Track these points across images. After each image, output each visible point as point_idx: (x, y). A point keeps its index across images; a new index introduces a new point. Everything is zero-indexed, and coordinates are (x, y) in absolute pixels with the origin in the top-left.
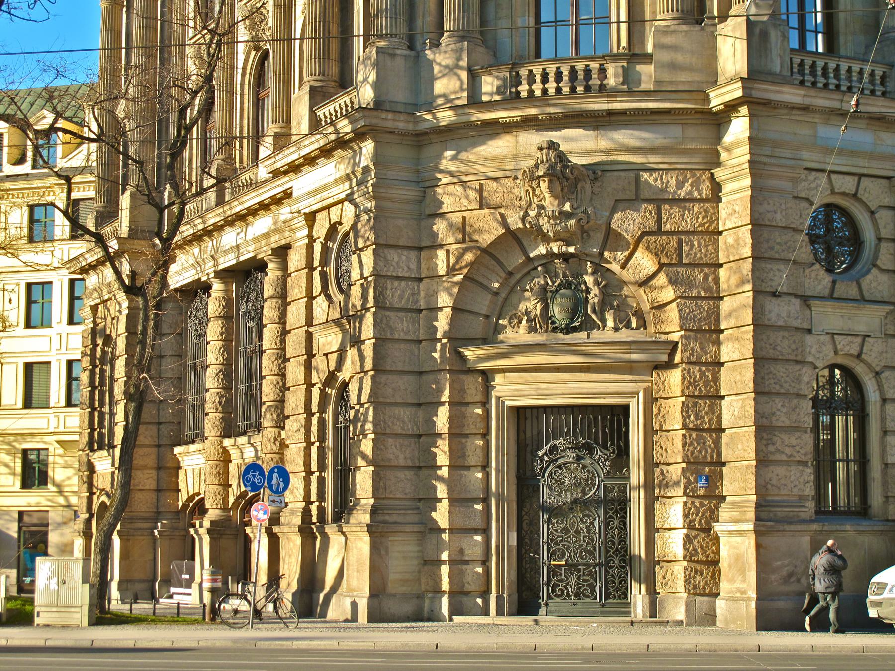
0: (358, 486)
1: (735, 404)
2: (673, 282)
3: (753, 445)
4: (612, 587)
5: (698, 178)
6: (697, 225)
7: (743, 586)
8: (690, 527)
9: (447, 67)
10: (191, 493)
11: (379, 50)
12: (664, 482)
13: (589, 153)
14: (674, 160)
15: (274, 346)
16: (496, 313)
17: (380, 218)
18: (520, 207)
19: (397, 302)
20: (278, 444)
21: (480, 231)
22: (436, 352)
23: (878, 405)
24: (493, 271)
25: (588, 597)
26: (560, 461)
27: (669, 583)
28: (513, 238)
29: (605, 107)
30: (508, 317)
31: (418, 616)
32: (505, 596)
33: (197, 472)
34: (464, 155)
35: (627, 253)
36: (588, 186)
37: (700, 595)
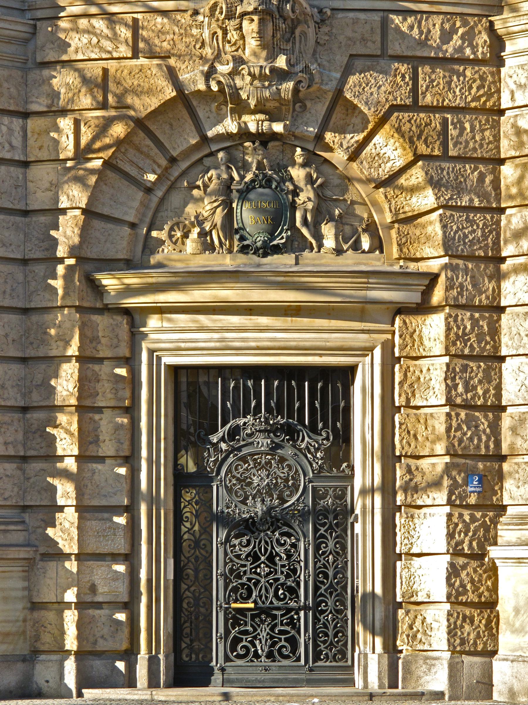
2: (434, 183)
4: (324, 642)
5: (472, 28)
6: (469, 99)
8: (456, 552)
12: (412, 484)
18: (201, 58)
22: (55, 277)
24: (148, 156)
25: (287, 657)
26: (245, 451)
27: (419, 636)
30: (167, 227)
32: (161, 656)
35: (360, 137)
36: (311, 32)
37: (469, 653)
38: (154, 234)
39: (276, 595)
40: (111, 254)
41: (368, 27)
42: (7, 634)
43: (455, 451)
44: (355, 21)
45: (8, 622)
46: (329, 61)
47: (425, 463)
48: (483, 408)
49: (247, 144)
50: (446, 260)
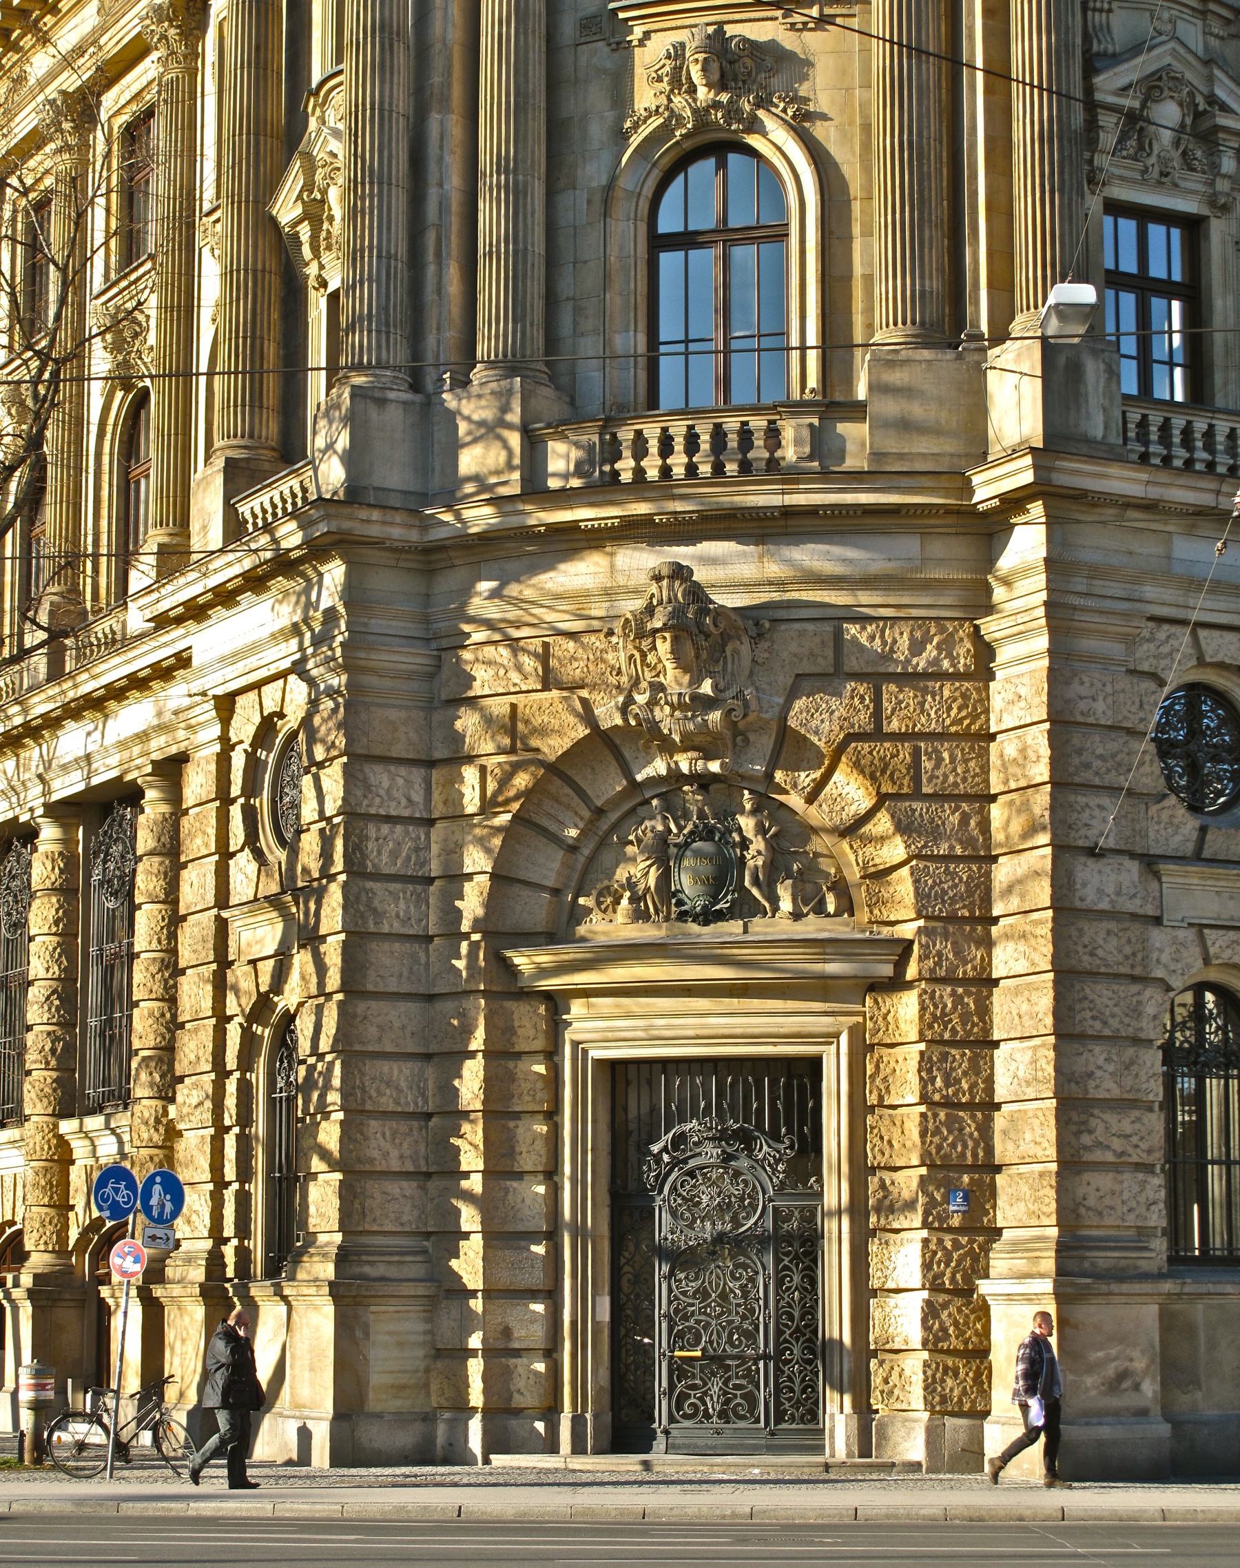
1: (1017, 1056)
2: (903, 827)
3: (1052, 1134)
4: (789, 1399)
5: (951, 635)
6: (948, 722)
8: (934, 1286)
9: (482, 424)
11: (356, 392)
12: (887, 1202)
15: (154, 945)
19: (386, 860)
22: (459, 958)
24: (568, 807)
25: (743, 1418)
26: (692, 1163)
27: (896, 1392)
29: (777, 500)
32: (588, 1416)
34: (513, 590)
35: (817, 774)
36: (745, 649)
37: (953, 1414)
38: (581, 901)
39: (730, 1341)
40: (529, 927)
41: (817, 640)
42: (403, 1387)
43: (932, 1160)
44: (801, 633)
45: (405, 1372)
46: (770, 684)
47: (899, 1176)
48: (970, 1106)
49: (686, 788)
50: (921, 923)
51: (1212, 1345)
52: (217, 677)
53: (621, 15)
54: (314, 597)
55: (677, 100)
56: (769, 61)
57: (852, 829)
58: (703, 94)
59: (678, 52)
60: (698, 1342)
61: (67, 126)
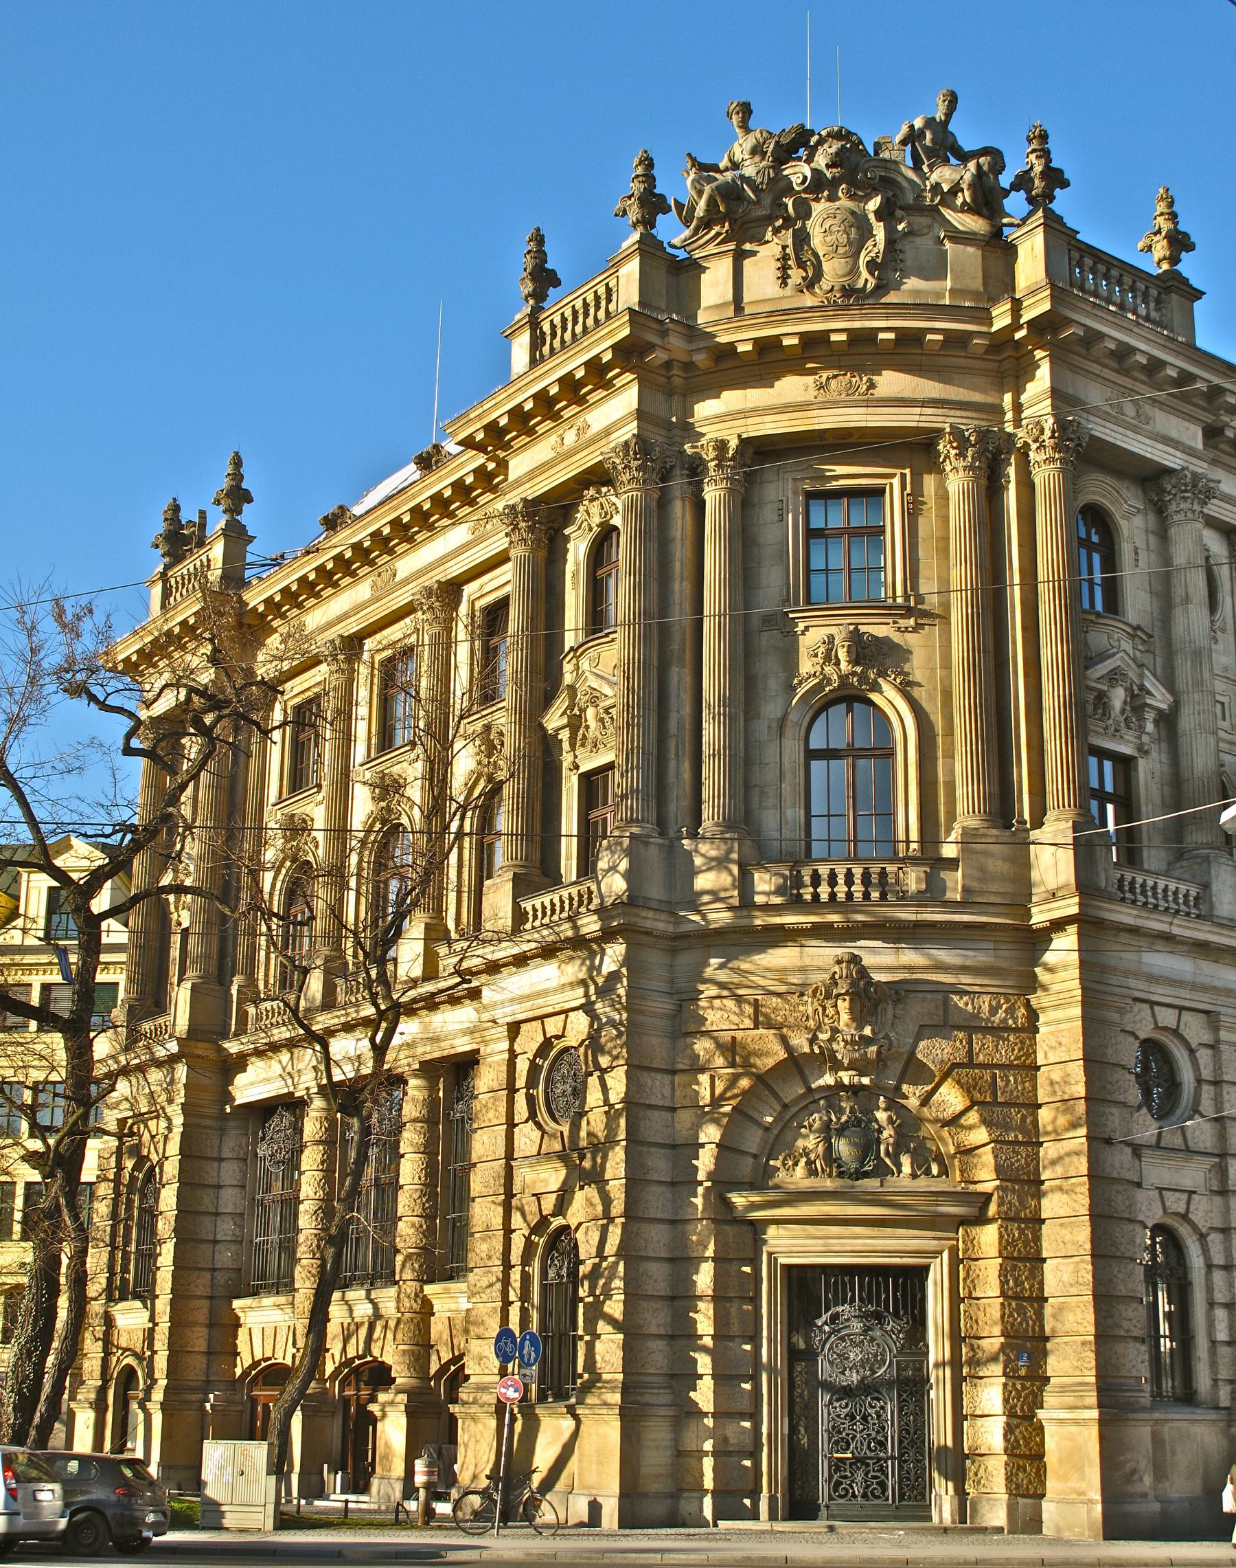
0: (598, 1358)
1: (1063, 1268)
2: (986, 1122)
3: (1091, 1317)
7: (1082, 1486)
9: (712, 859)
10: (258, 1356)
11: (632, 837)
13: (890, 969)
14: (986, 982)
15: (416, 1181)
16: (766, 1152)
17: (633, 1033)
19: (653, 1134)
20: (419, 1301)
21: (759, 1054)
23: (1203, 1272)
25: (878, 1497)
28: (796, 1065)
29: (912, 917)
31: (674, 1520)
32: (779, 1495)
33: (269, 1332)
34: (734, 964)
35: (929, 1087)
36: (890, 1009)
37: (1023, 1496)
38: (772, 1162)
48: (1030, 1299)
50: (998, 1182)
51: (1174, 1453)
52: (508, 1010)
53: (791, 615)
54: (597, 962)
55: (827, 669)
56: (885, 649)
57: (953, 1121)
58: (844, 666)
59: (831, 638)
60: (848, 1448)
61: (341, 657)
